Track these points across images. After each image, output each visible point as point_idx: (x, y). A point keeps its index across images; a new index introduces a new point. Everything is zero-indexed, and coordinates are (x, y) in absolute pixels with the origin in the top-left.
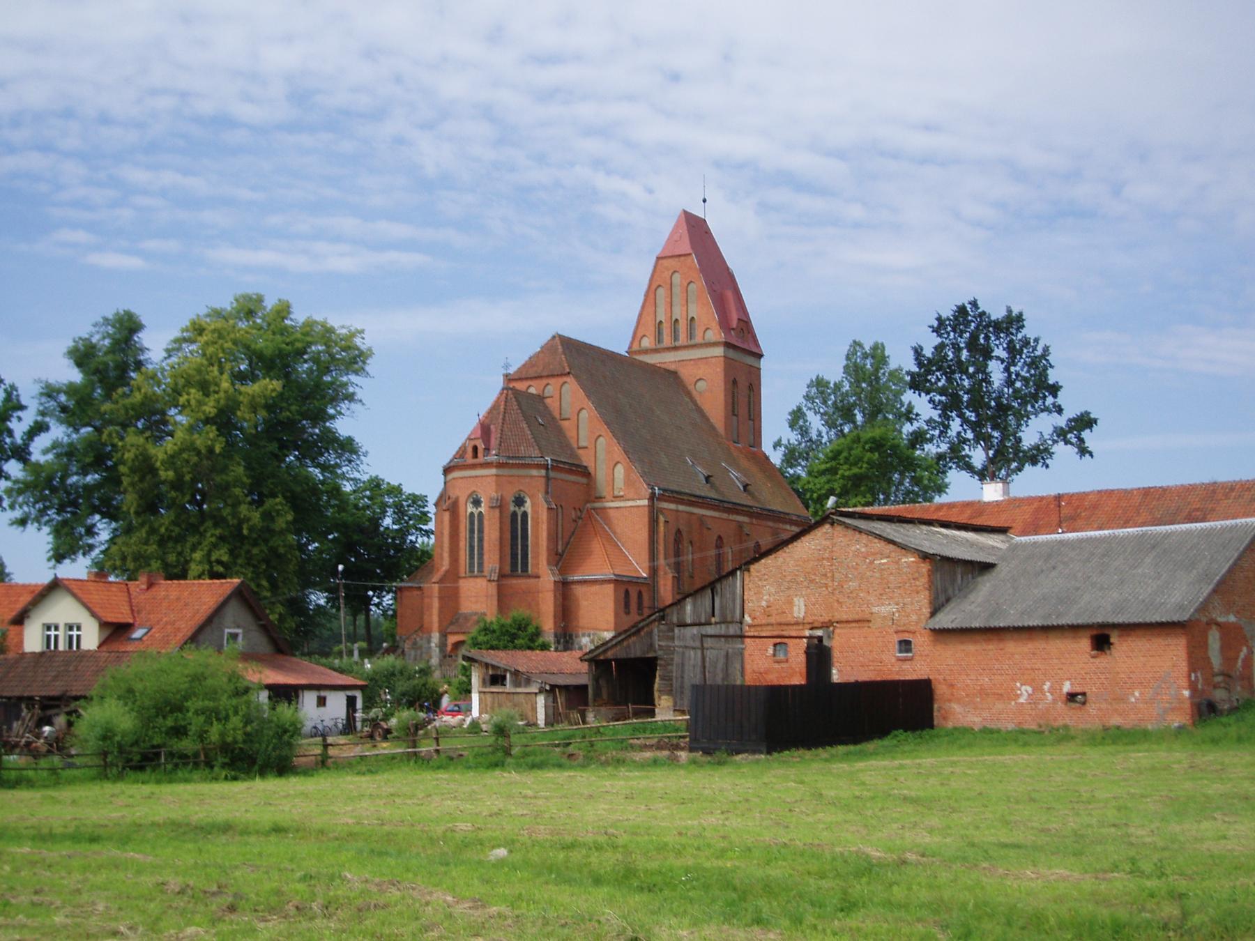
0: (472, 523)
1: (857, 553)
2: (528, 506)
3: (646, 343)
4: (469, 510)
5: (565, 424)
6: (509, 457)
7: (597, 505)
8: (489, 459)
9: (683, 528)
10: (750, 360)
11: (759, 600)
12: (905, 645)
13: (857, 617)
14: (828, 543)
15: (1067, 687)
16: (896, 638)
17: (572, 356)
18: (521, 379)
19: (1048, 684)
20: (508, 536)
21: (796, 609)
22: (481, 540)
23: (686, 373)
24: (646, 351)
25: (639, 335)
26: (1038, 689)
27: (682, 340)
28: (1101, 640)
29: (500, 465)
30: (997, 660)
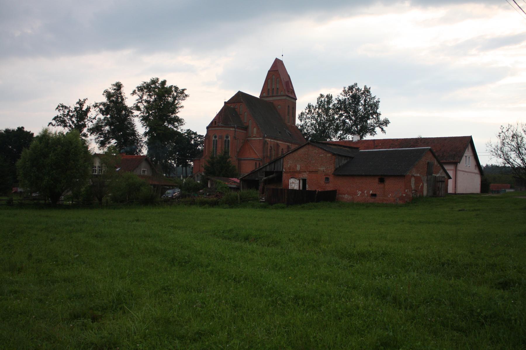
2: (229, 139)
3: (264, 95)
9: (272, 146)
10: (293, 100)
12: (327, 179)
15: (371, 192)
16: (324, 177)
17: (241, 98)
24: (264, 97)
26: (363, 192)
28: (382, 180)
29: (222, 127)
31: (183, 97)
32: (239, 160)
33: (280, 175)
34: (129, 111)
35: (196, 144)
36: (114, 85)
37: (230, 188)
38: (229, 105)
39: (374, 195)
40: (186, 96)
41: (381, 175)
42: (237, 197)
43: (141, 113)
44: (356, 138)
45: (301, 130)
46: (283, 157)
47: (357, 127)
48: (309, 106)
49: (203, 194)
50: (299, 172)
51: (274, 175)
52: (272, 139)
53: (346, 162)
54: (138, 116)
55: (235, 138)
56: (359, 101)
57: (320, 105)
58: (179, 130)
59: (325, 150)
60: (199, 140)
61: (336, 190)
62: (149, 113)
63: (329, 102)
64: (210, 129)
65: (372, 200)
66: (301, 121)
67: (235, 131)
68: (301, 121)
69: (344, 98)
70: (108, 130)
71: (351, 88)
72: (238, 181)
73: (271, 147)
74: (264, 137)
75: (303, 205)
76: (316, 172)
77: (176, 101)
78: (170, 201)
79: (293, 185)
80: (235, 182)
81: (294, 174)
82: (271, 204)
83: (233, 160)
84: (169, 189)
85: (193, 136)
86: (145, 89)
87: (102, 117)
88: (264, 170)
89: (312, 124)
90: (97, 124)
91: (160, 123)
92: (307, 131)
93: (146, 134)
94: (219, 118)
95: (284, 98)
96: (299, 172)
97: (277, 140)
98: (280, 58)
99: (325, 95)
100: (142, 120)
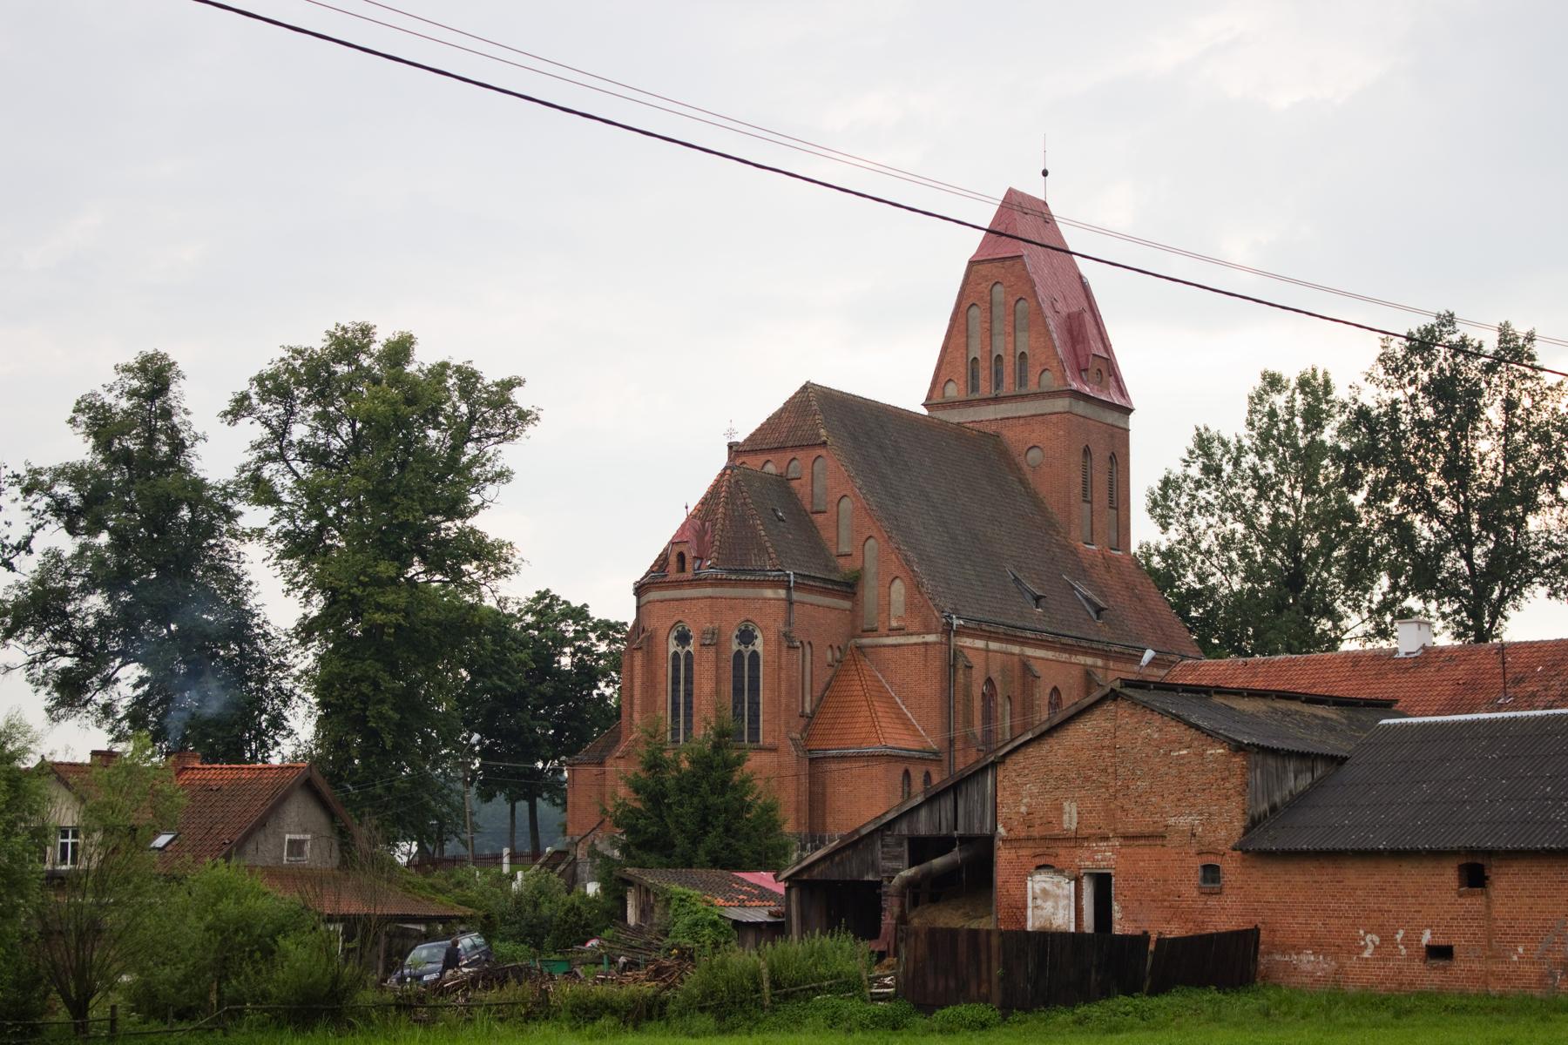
0: (676, 669)
1: (1148, 740)
2: (759, 645)
3: (952, 391)
4: (672, 650)
5: (819, 519)
6: (730, 571)
7: (866, 641)
8: (705, 572)
9: (995, 676)
10: (1112, 418)
11: (1017, 803)
13: (1147, 831)
14: (1109, 725)
16: (1198, 863)
17: (821, 420)
18: (754, 451)
19: (1401, 932)
20: (728, 688)
21: (1066, 817)
22: (689, 694)
23: (1010, 435)
25: (943, 379)
26: (1387, 939)
27: (1008, 386)
28: (1474, 878)
29: (718, 582)
30: (1333, 896)
31: (506, 422)
32: (815, 762)
33: (981, 852)
34: (213, 510)
35: (587, 674)
36: (127, 369)
37: (737, 924)
38: (754, 462)
39: (1440, 953)
40: (523, 416)
41: (1471, 852)
42: (755, 977)
43: (282, 514)
44: (1434, 628)
45: (1165, 580)
46: (994, 765)
47: (1468, 557)
48: (1203, 443)
49: (597, 962)
50: (1077, 840)
51: (955, 855)
52: (990, 636)
53: (1305, 780)
54: (260, 533)
55: (788, 640)
56: (1474, 413)
57: (1265, 436)
58: (490, 602)
59: (1198, 728)
60: (603, 647)
61: (1256, 931)
62: (321, 515)
63: (1314, 418)
64: (654, 595)
65: (1431, 977)
66: (1165, 528)
67: (790, 602)
68: (1165, 528)
69: (1387, 396)
70: (99, 614)
71: (1422, 344)
72: (780, 888)
73: (989, 681)
74: (948, 630)
75: (1081, 1010)
76: (1156, 837)
77: (471, 449)
78: (416, 1006)
79: (1049, 905)
80: (764, 894)
81: (1048, 850)
82: (926, 1006)
83: (769, 773)
84: (427, 938)
85: (569, 628)
86: (299, 384)
87: (68, 545)
88: (903, 828)
89: (1226, 543)
90: (41, 582)
91: (385, 568)
92: (1202, 578)
93: (306, 630)
94: (700, 534)
95: (1061, 404)
96: (1077, 840)
97: (1024, 642)
98: (1033, 188)
99: (1291, 375)
100: (284, 555)
